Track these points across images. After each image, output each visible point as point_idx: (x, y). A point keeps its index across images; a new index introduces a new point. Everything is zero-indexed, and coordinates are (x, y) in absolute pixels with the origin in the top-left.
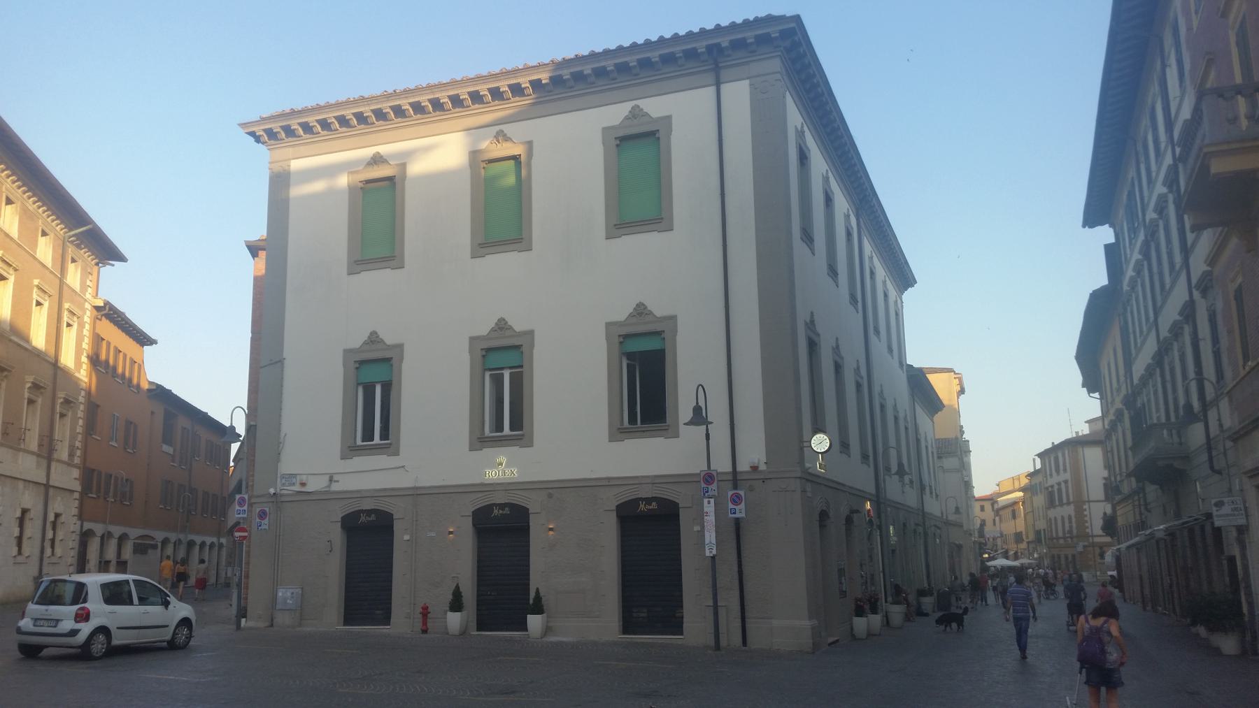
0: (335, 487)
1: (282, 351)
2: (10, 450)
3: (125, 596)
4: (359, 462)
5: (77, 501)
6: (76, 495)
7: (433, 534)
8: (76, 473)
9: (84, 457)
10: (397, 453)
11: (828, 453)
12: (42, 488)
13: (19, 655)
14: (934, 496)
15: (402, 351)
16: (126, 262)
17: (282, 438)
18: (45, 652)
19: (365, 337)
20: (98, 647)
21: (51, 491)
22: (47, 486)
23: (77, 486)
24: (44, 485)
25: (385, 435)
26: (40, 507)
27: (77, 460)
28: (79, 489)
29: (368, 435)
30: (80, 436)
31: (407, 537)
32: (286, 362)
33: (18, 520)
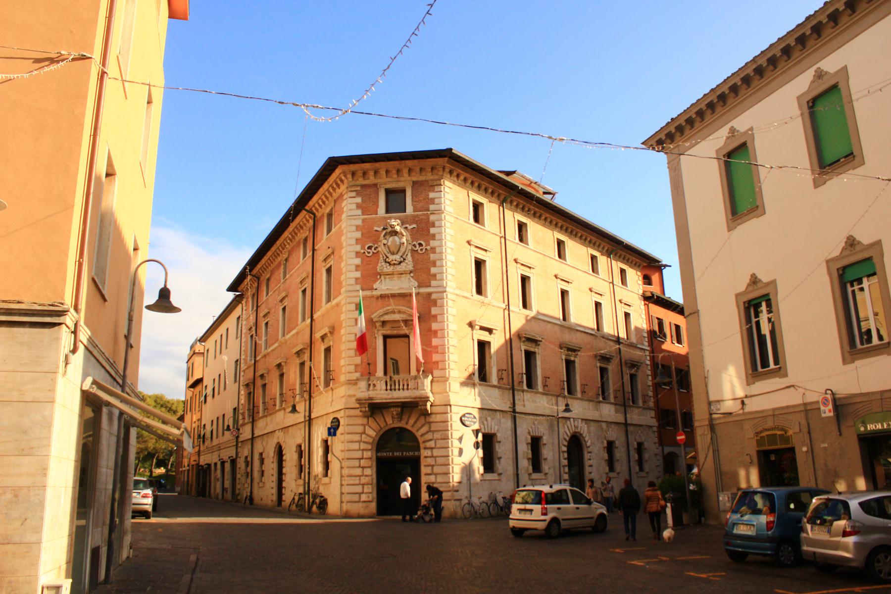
0: (748, 409)
1: (157, 300)
2: (591, 403)
3: (564, 498)
4: (761, 386)
5: (656, 433)
6: (655, 429)
7: (826, 445)
8: (653, 413)
9: (657, 402)
10: (786, 375)
11: (167, 267)
12: (623, 427)
13: (511, 536)
14: (61, 305)
15: (776, 286)
16: (754, 274)
17: (706, 373)
18: (526, 533)
19: (747, 280)
20: (555, 532)
21: (630, 429)
22: (626, 424)
23: (654, 422)
24: (624, 424)
25: (776, 362)
26: (623, 439)
27: (651, 404)
28: (656, 424)
29: (765, 364)
30: (651, 388)
31: (805, 449)
32: (701, 313)
33: (606, 449)
